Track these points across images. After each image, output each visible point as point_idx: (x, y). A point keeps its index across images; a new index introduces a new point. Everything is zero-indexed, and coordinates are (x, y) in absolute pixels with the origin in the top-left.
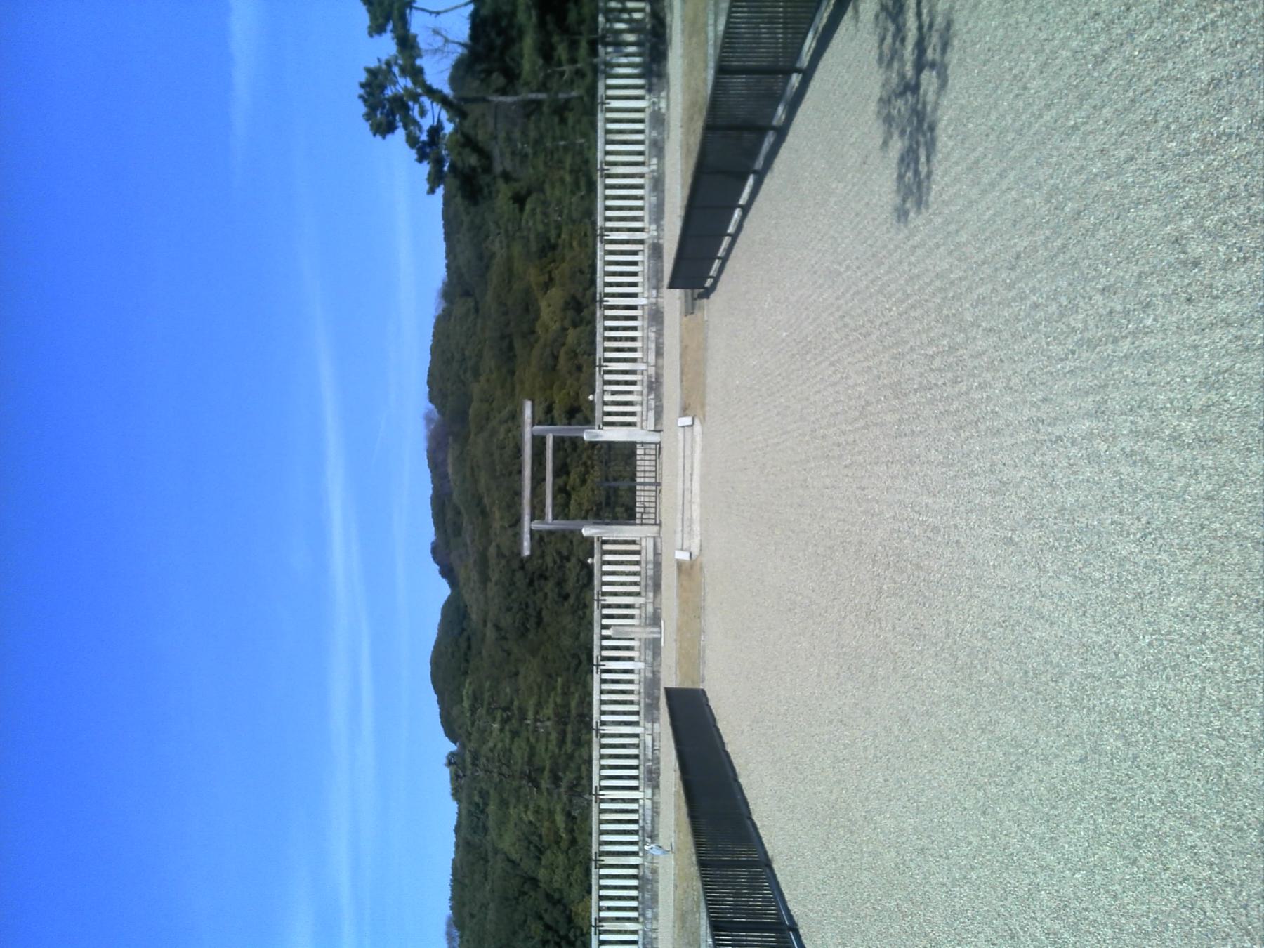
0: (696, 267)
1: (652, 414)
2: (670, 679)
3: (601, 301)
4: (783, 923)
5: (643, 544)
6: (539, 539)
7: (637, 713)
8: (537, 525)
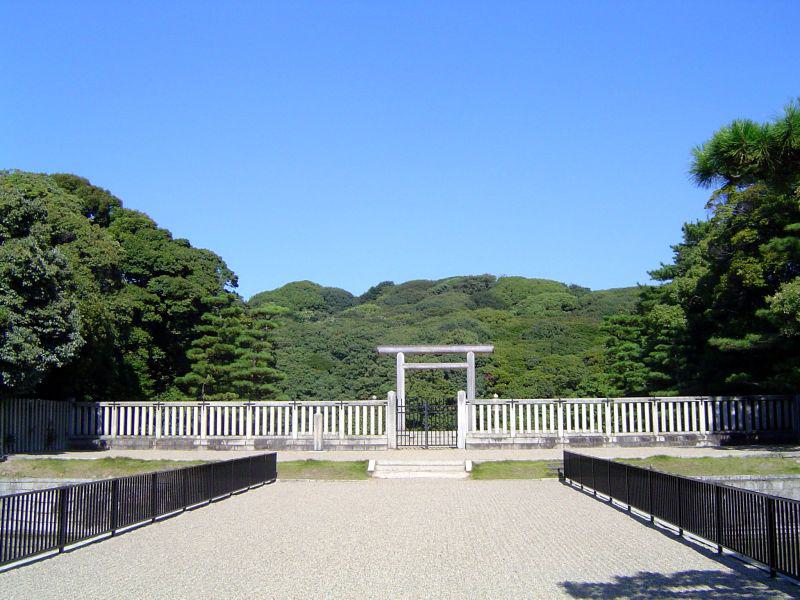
0: (579, 470)
1: (478, 441)
2: (282, 457)
3: (249, 404)
4: (66, 544)
5: (383, 437)
7: (261, 434)
8: (401, 358)
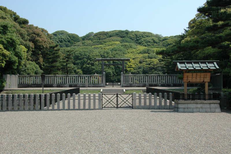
1: (126, 85)
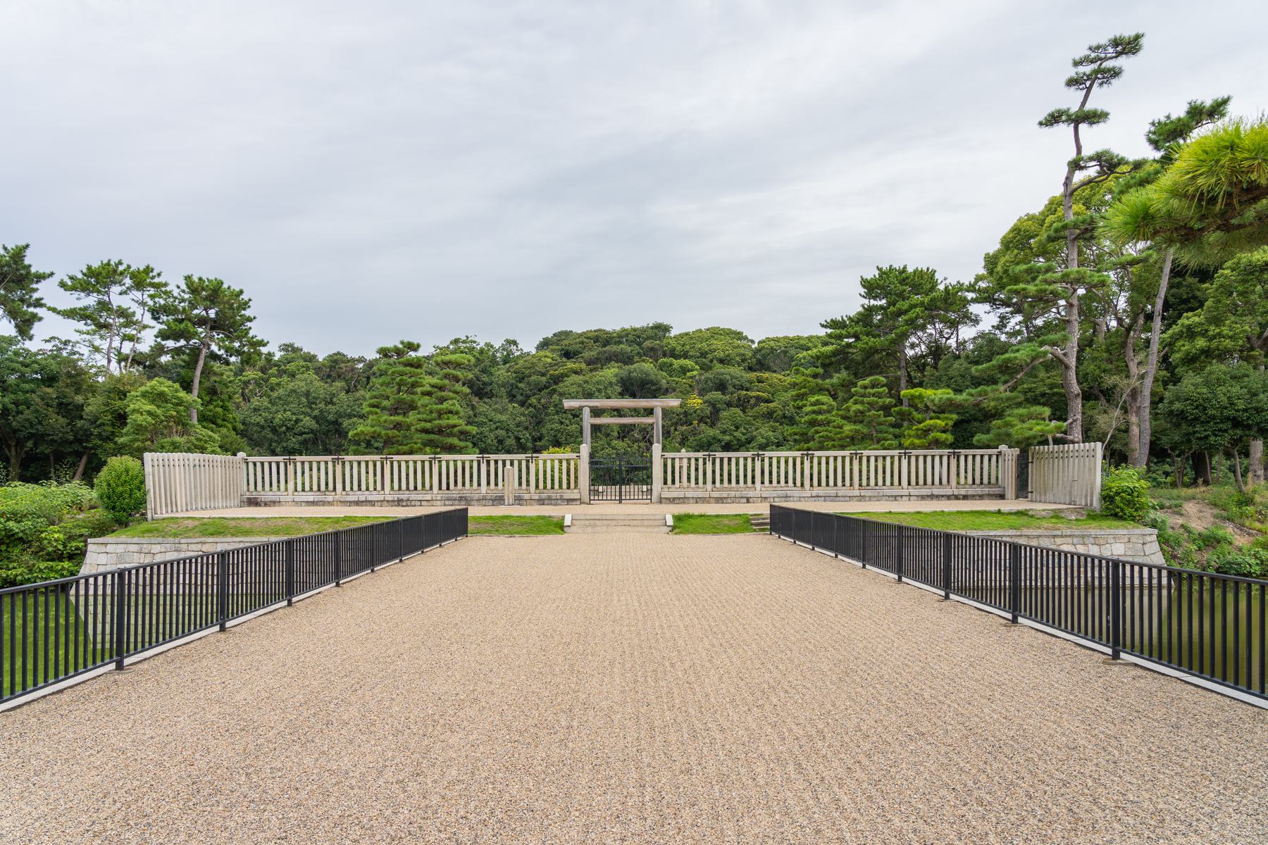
0: (787, 523)
2: (473, 512)
6: (576, 414)
